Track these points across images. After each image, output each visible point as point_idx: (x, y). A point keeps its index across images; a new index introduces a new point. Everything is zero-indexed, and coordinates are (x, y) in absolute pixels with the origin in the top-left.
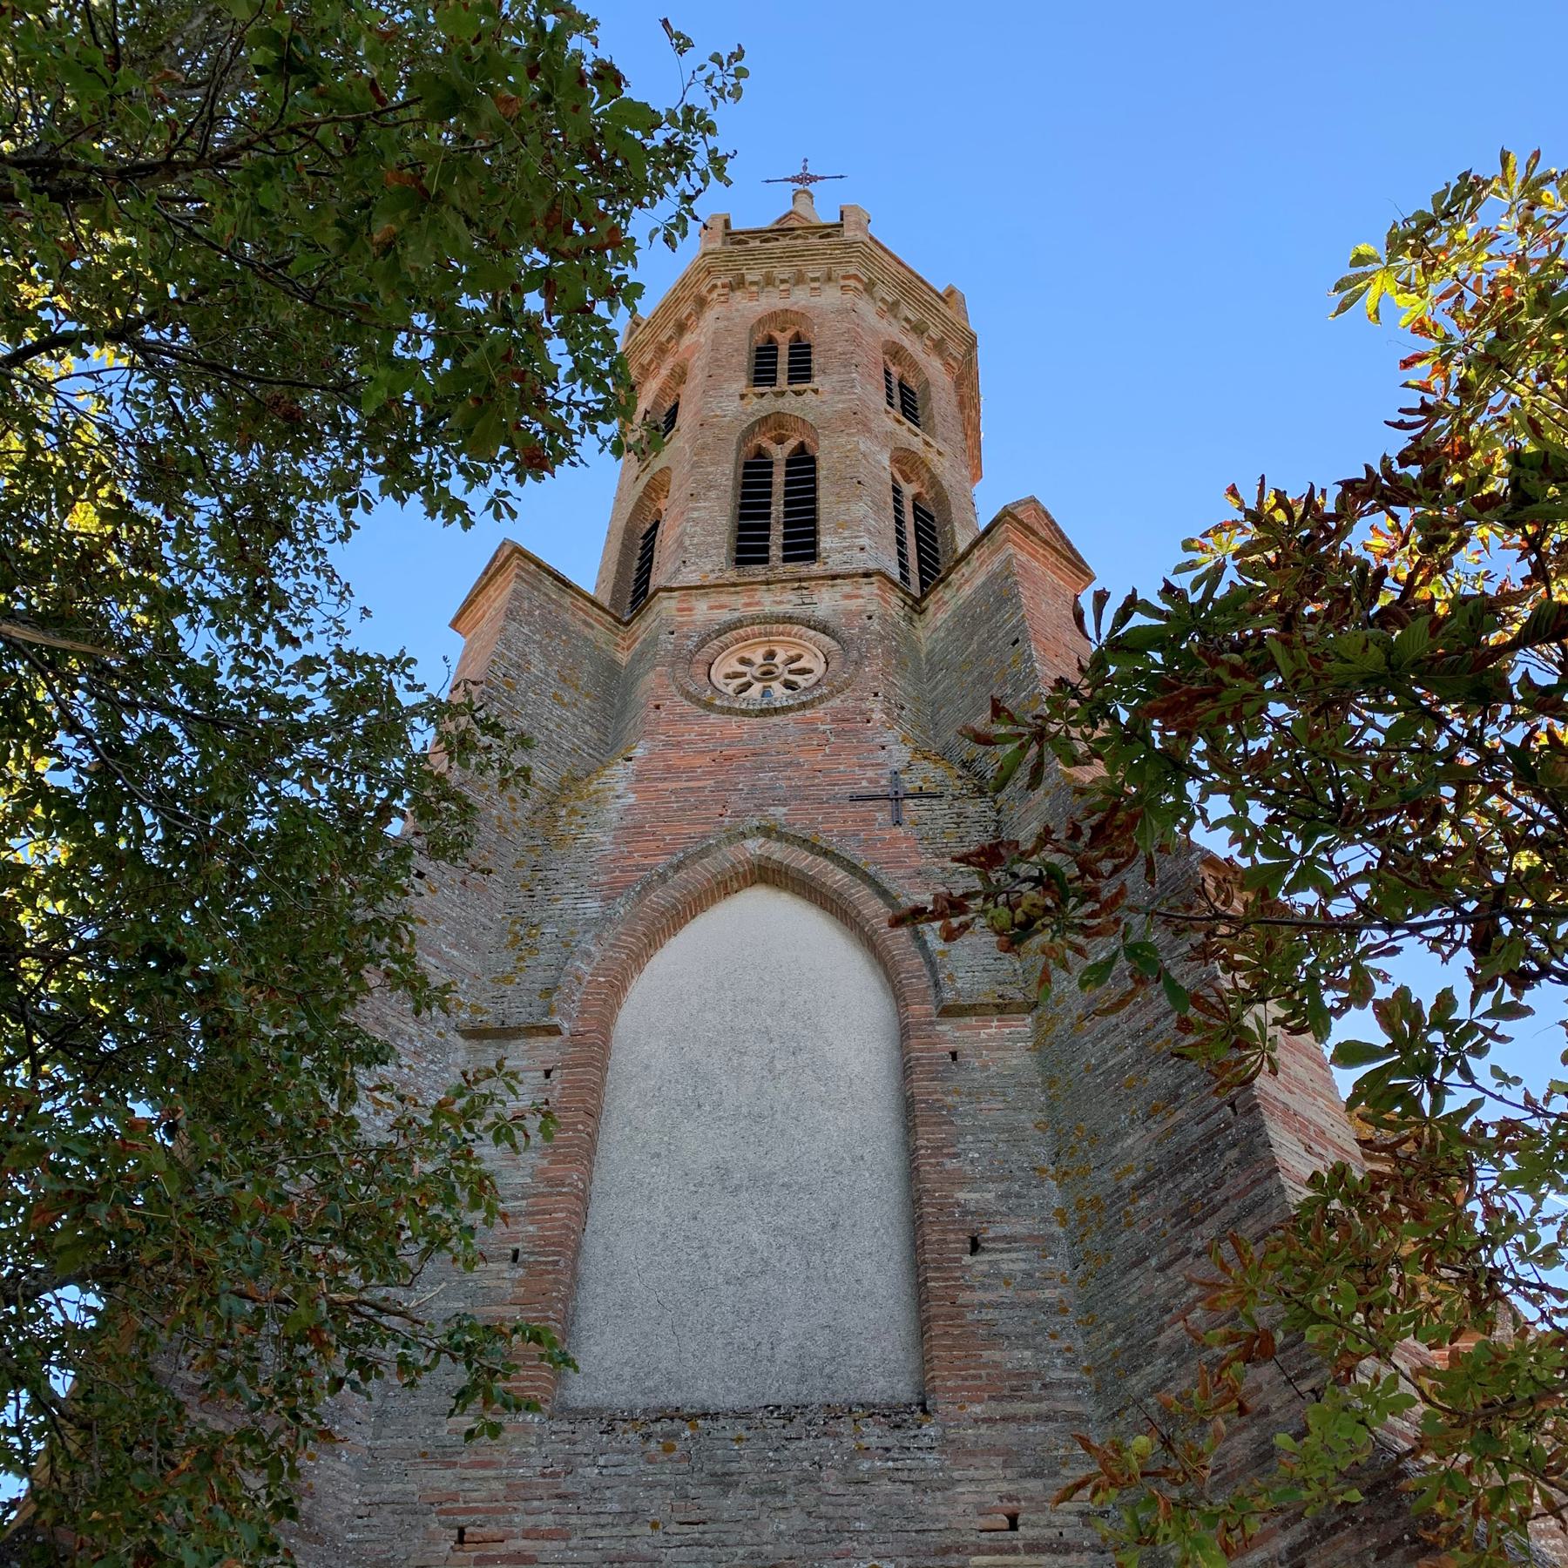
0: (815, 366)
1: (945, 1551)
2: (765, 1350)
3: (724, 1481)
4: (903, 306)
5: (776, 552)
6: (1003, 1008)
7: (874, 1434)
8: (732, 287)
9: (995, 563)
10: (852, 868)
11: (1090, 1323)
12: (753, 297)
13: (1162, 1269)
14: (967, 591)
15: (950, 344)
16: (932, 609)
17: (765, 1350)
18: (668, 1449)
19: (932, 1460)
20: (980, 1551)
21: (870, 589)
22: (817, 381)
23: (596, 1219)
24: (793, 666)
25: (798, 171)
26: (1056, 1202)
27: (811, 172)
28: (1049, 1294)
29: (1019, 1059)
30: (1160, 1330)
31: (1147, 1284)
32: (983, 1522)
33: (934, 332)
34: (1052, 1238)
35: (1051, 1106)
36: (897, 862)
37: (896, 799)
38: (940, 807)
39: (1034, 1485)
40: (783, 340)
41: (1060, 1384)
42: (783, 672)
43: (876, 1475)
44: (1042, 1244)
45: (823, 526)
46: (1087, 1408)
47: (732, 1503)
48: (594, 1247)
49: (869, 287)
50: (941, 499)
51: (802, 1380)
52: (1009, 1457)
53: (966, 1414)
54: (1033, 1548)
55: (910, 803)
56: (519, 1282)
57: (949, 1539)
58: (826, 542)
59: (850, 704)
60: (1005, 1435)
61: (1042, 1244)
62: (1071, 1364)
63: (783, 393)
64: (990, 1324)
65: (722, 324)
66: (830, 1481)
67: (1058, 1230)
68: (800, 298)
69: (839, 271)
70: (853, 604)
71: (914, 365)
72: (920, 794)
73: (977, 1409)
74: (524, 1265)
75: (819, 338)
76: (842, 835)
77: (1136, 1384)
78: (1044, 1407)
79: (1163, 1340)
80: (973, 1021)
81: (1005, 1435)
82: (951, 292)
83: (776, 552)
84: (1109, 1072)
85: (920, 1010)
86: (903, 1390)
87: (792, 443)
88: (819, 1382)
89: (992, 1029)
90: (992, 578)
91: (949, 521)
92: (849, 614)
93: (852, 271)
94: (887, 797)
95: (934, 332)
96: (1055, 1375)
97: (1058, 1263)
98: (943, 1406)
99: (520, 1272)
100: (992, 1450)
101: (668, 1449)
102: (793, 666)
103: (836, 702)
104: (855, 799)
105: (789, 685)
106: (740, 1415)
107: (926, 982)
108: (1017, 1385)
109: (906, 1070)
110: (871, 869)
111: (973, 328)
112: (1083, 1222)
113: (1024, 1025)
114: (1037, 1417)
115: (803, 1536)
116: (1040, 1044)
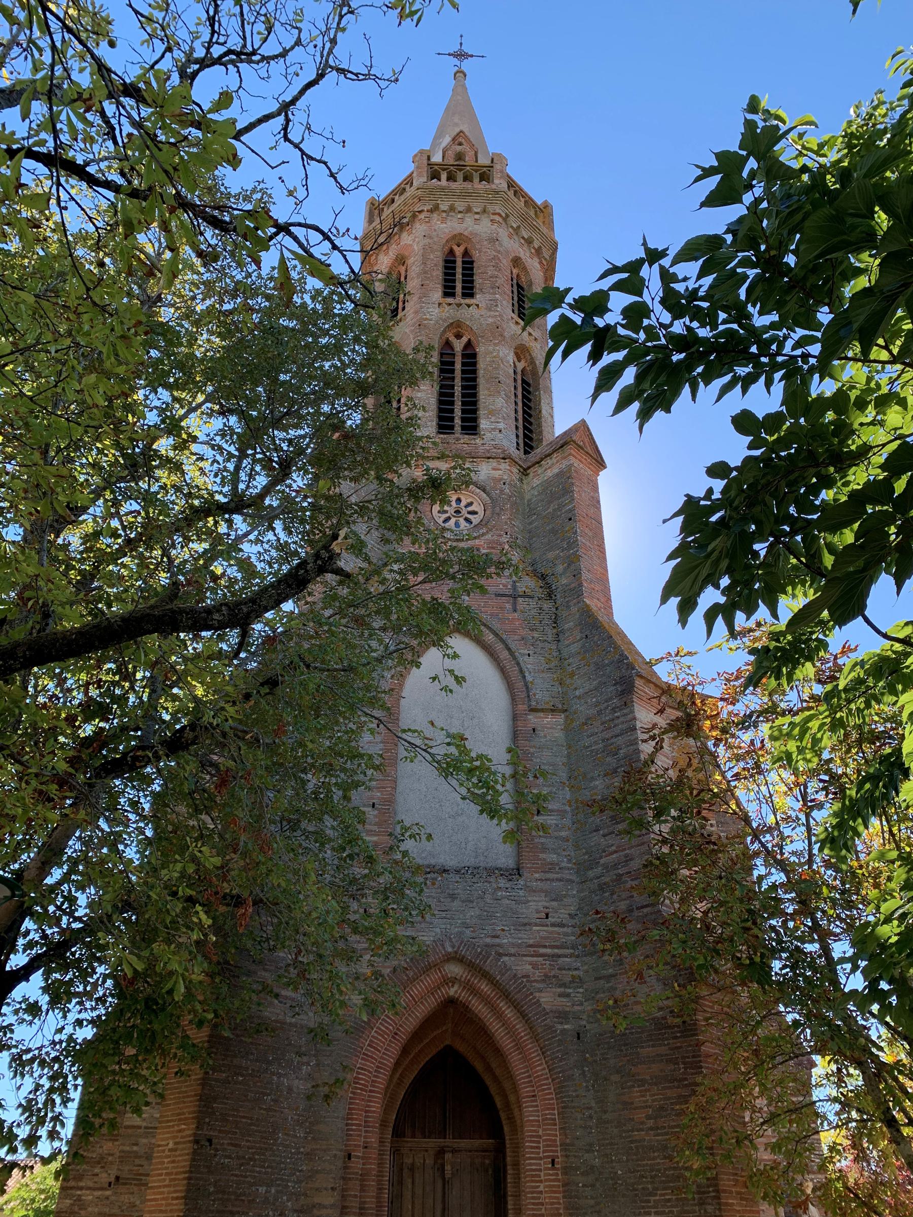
0: (476, 290)
1: (525, 925)
2: (463, 845)
3: (453, 897)
4: (522, 229)
5: (458, 428)
6: (553, 710)
7: (502, 883)
8: (431, 211)
9: (564, 464)
10: (496, 635)
11: (577, 847)
12: (444, 221)
13: (604, 836)
14: (549, 473)
15: (544, 250)
16: (531, 475)
17: (463, 845)
18: (433, 884)
19: (521, 893)
20: (536, 925)
21: (505, 466)
22: (479, 298)
23: (400, 788)
24: (470, 509)
25: (456, 48)
26: (568, 797)
27: (466, 49)
28: (563, 834)
29: (559, 734)
30: (601, 858)
31: (596, 839)
32: (538, 915)
33: (536, 244)
34: (565, 811)
35: (569, 756)
36: (514, 631)
37: (514, 597)
38: (533, 603)
39: (555, 904)
40: (459, 251)
41: (565, 868)
42: (464, 512)
43: (503, 897)
44: (562, 813)
45: (482, 412)
46: (574, 878)
47: (456, 903)
48: (400, 799)
49: (506, 219)
50: (534, 373)
51: (476, 857)
52: (547, 893)
53: (531, 877)
54: (553, 925)
55: (520, 600)
56: (376, 816)
57: (526, 921)
58: (484, 424)
59: (495, 538)
60: (546, 886)
61: (562, 813)
62: (569, 861)
63: (459, 305)
64: (542, 844)
65: (427, 241)
66: (488, 898)
67: (568, 808)
68: (468, 225)
69: (490, 208)
70: (497, 474)
71: (525, 269)
72: (525, 595)
73: (537, 875)
74: (378, 809)
75: (481, 259)
76: (492, 615)
77: (591, 874)
78: (559, 876)
79: (602, 861)
80: (542, 714)
81: (546, 886)
82: (546, 205)
83: (458, 428)
84: (592, 751)
85: (522, 707)
86: (511, 863)
87: (465, 340)
88: (482, 858)
89: (549, 719)
90: (561, 474)
91: (538, 389)
92: (497, 480)
93: (498, 211)
94: (510, 596)
95: (536, 244)
96: (564, 865)
97: (567, 821)
98: (526, 874)
99: (376, 812)
100: (541, 891)
101: (433, 884)
102: (470, 509)
103: (488, 537)
104: (498, 595)
105: (467, 520)
106: (458, 871)
107: (524, 695)
108: (551, 867)
109: (515, 735)
110: (504, 637)
111: (557, 238)
112: (577, 808)
113: (560, 719)
114: (557, 880)
115: (479, 917)
116: (567, 729)
